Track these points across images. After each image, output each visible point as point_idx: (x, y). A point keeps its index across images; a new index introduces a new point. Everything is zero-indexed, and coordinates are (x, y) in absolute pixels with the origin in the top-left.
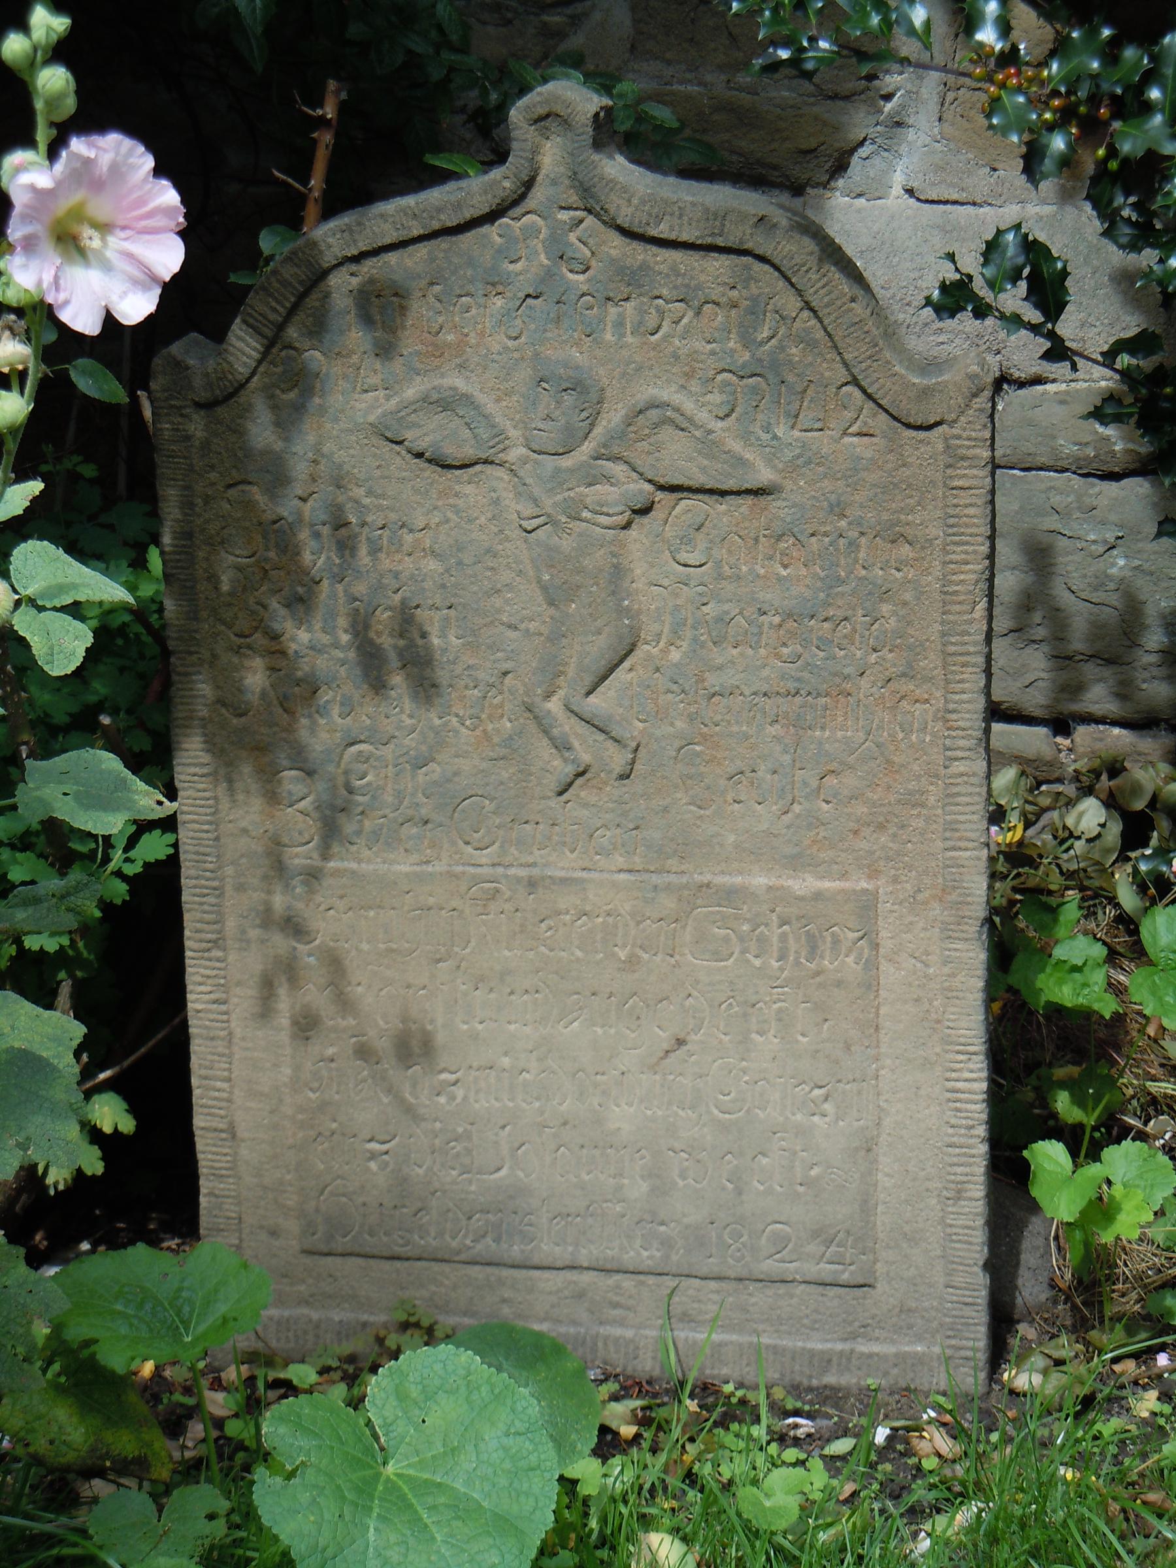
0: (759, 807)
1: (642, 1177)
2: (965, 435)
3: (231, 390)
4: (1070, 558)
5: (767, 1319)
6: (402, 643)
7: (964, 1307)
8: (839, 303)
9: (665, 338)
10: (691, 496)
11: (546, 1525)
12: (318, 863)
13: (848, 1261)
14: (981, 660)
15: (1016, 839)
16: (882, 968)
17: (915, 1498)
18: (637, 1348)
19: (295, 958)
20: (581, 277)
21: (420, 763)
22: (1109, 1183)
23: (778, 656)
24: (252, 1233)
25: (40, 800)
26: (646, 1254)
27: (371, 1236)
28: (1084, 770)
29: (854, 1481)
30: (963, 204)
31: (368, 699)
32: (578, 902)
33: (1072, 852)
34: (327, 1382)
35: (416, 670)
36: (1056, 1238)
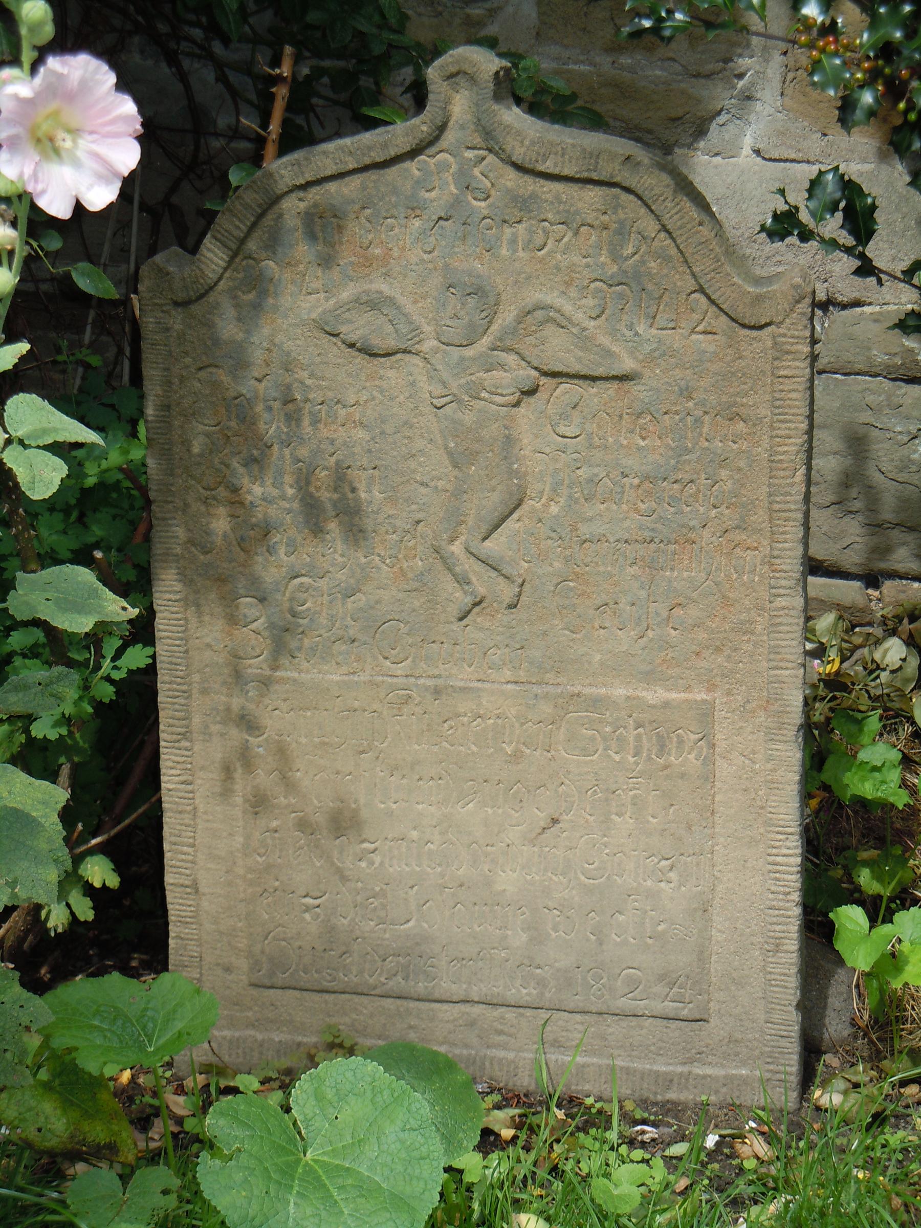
0: (620, 633)
1: (522, 930)
2: (789, 334)
3: (202, 291)
4: (881, 446)
5: (622, 1046)
6: (336, 496)
7: (780, 1039)
8: (689, 226)
9: (549, 254)
10: (568, 380)
11: (433, 1204)
12: (268, 672)
13: (687, 1000)
14: (800, 516)
15: (834, 670)
16: (717, 764)
17: (737, 1191)
18: (517, 1067)
19: (247, 748)
20: (483, 204)
21: (349, 594)
22: (900, 941)
23: (637, 511)
24: (210, 969)
25: (27, 603)
26: (524, 991)
27: (306, 973)
28: (890, 616)
29: (688, 1177)
30: (799, 162)
31: (308, 541)
32: (474, 707)
33: (878, 681)
34: (268, 1089)
35: (347, 518)
36: (857, 986)
